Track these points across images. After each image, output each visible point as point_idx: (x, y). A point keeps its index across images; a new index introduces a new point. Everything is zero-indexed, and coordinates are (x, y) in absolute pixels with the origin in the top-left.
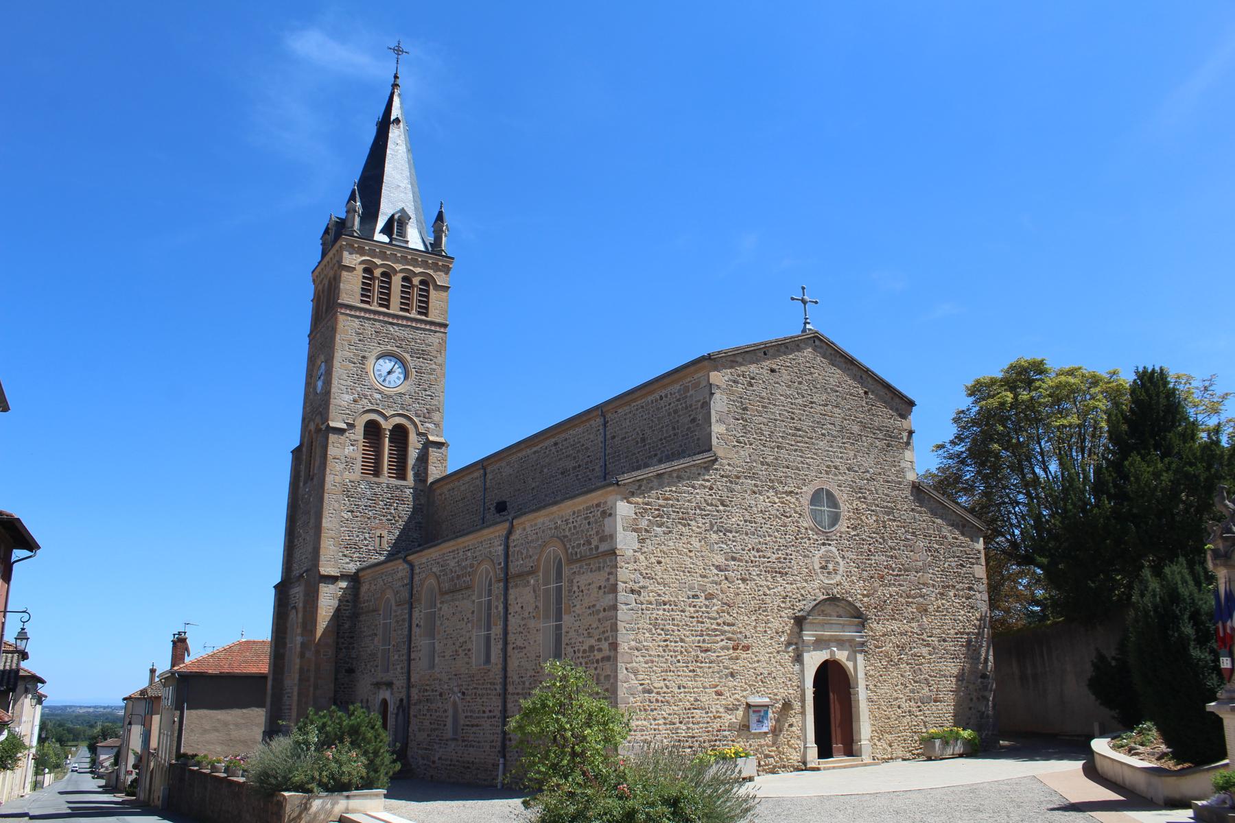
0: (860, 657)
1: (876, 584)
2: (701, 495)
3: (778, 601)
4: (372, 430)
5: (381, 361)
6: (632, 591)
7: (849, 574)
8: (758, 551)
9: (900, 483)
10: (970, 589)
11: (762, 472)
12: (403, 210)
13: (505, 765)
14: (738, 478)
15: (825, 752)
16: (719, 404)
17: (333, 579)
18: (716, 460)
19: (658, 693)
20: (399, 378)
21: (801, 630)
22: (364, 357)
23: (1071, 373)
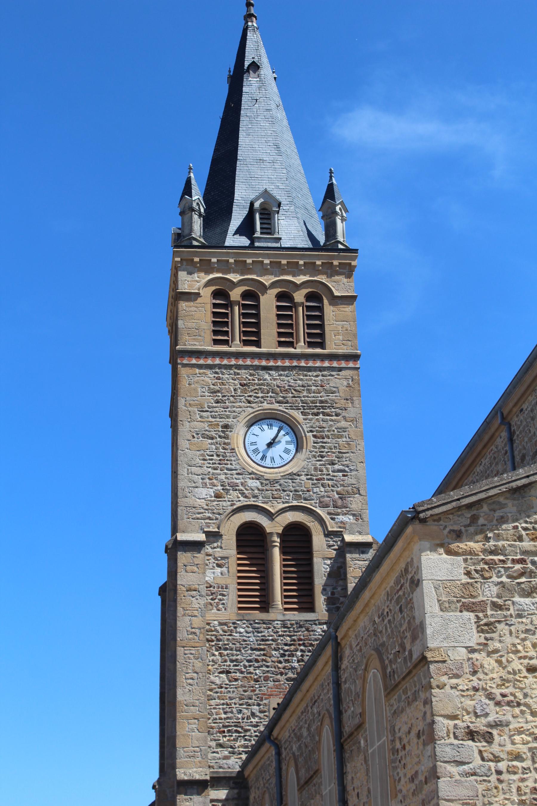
4: (251, 539)
5: (255, 429)
6: (472, 735)
12: (266, 193)
17: (198, 786)
20: (287, 451)
22: (226, 426)
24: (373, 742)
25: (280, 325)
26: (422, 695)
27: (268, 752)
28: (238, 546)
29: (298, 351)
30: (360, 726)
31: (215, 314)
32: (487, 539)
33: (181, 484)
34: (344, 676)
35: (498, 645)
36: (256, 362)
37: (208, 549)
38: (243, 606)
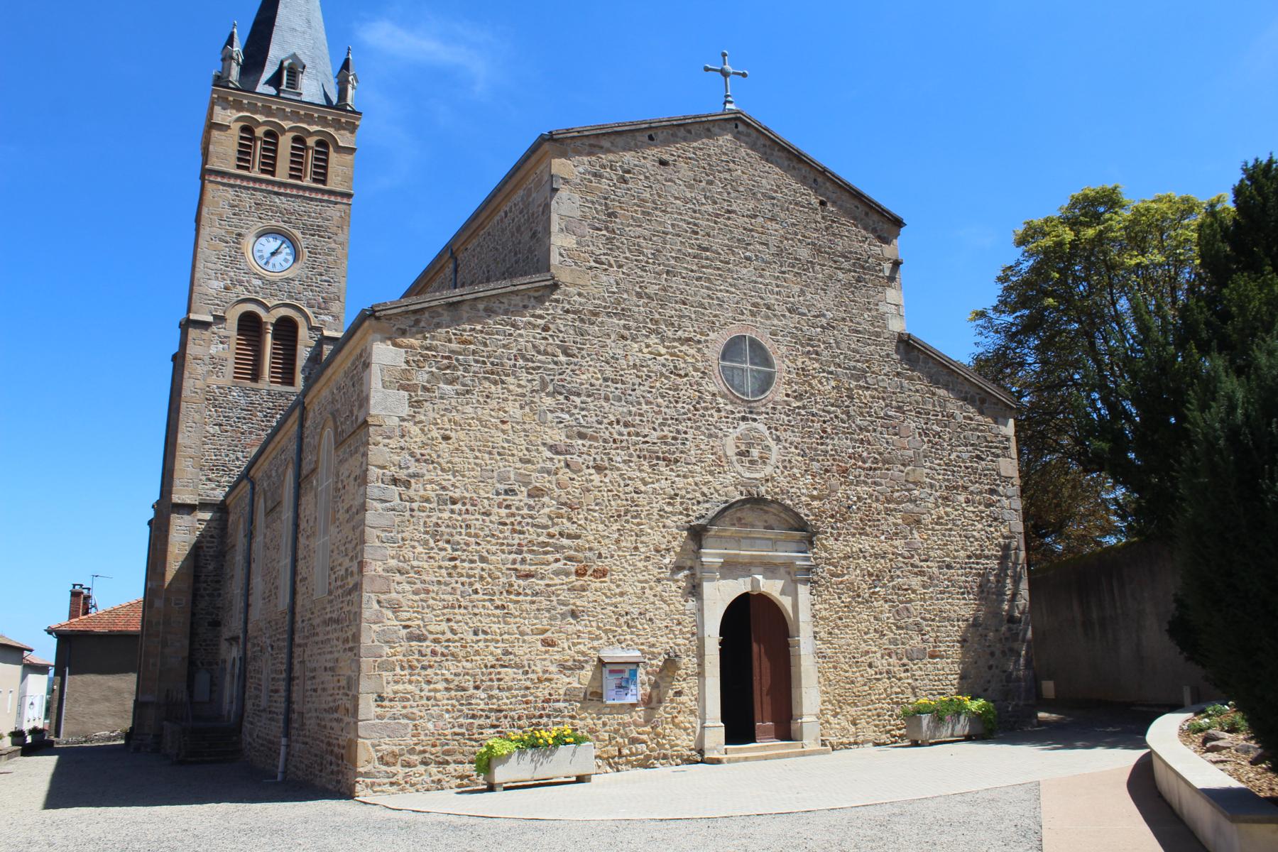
0: (803, 590)
1: (833, 481)
2: (526, 337)
3: (660, 503)
4: (250, 326)
5: (263, 240)
6: (395, 481)
7: (787, 465)
8: (626, 425)
9: (878, 335)
10: (992, 492)
11: (639, 308)
12: (294, 56)
13: (288, 746)
14: (596, 315)
15: (739, 728)
16: (565, 205)
17: (189, 509)
18: (556, 286)
19: (436, 641)
20: (286, 260)
21: (700, 547)
22: (239, 235)
23: (1159, 200)
24: (323, 483)
25: (292, 162)
26: (362, 449)
27: (246, 486)
28: (239, 330)
29: (304, 184)
30: (314, 470)
31: (241, 145)
32: (425, 338)
33: (197, 275)
34: (307, 432)
35: (423, 418)
36: (270, 188)
37: (214, 328)
38: (238, 375)
